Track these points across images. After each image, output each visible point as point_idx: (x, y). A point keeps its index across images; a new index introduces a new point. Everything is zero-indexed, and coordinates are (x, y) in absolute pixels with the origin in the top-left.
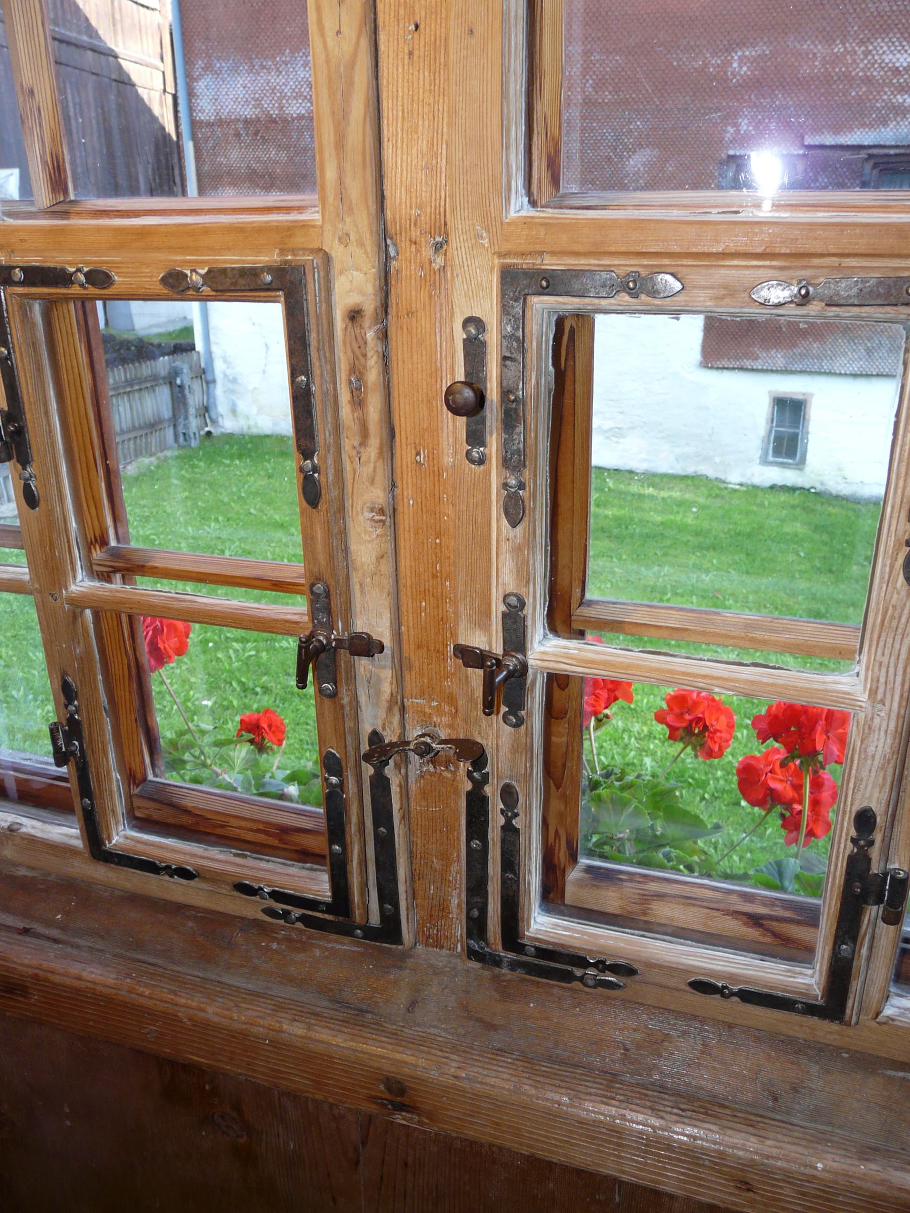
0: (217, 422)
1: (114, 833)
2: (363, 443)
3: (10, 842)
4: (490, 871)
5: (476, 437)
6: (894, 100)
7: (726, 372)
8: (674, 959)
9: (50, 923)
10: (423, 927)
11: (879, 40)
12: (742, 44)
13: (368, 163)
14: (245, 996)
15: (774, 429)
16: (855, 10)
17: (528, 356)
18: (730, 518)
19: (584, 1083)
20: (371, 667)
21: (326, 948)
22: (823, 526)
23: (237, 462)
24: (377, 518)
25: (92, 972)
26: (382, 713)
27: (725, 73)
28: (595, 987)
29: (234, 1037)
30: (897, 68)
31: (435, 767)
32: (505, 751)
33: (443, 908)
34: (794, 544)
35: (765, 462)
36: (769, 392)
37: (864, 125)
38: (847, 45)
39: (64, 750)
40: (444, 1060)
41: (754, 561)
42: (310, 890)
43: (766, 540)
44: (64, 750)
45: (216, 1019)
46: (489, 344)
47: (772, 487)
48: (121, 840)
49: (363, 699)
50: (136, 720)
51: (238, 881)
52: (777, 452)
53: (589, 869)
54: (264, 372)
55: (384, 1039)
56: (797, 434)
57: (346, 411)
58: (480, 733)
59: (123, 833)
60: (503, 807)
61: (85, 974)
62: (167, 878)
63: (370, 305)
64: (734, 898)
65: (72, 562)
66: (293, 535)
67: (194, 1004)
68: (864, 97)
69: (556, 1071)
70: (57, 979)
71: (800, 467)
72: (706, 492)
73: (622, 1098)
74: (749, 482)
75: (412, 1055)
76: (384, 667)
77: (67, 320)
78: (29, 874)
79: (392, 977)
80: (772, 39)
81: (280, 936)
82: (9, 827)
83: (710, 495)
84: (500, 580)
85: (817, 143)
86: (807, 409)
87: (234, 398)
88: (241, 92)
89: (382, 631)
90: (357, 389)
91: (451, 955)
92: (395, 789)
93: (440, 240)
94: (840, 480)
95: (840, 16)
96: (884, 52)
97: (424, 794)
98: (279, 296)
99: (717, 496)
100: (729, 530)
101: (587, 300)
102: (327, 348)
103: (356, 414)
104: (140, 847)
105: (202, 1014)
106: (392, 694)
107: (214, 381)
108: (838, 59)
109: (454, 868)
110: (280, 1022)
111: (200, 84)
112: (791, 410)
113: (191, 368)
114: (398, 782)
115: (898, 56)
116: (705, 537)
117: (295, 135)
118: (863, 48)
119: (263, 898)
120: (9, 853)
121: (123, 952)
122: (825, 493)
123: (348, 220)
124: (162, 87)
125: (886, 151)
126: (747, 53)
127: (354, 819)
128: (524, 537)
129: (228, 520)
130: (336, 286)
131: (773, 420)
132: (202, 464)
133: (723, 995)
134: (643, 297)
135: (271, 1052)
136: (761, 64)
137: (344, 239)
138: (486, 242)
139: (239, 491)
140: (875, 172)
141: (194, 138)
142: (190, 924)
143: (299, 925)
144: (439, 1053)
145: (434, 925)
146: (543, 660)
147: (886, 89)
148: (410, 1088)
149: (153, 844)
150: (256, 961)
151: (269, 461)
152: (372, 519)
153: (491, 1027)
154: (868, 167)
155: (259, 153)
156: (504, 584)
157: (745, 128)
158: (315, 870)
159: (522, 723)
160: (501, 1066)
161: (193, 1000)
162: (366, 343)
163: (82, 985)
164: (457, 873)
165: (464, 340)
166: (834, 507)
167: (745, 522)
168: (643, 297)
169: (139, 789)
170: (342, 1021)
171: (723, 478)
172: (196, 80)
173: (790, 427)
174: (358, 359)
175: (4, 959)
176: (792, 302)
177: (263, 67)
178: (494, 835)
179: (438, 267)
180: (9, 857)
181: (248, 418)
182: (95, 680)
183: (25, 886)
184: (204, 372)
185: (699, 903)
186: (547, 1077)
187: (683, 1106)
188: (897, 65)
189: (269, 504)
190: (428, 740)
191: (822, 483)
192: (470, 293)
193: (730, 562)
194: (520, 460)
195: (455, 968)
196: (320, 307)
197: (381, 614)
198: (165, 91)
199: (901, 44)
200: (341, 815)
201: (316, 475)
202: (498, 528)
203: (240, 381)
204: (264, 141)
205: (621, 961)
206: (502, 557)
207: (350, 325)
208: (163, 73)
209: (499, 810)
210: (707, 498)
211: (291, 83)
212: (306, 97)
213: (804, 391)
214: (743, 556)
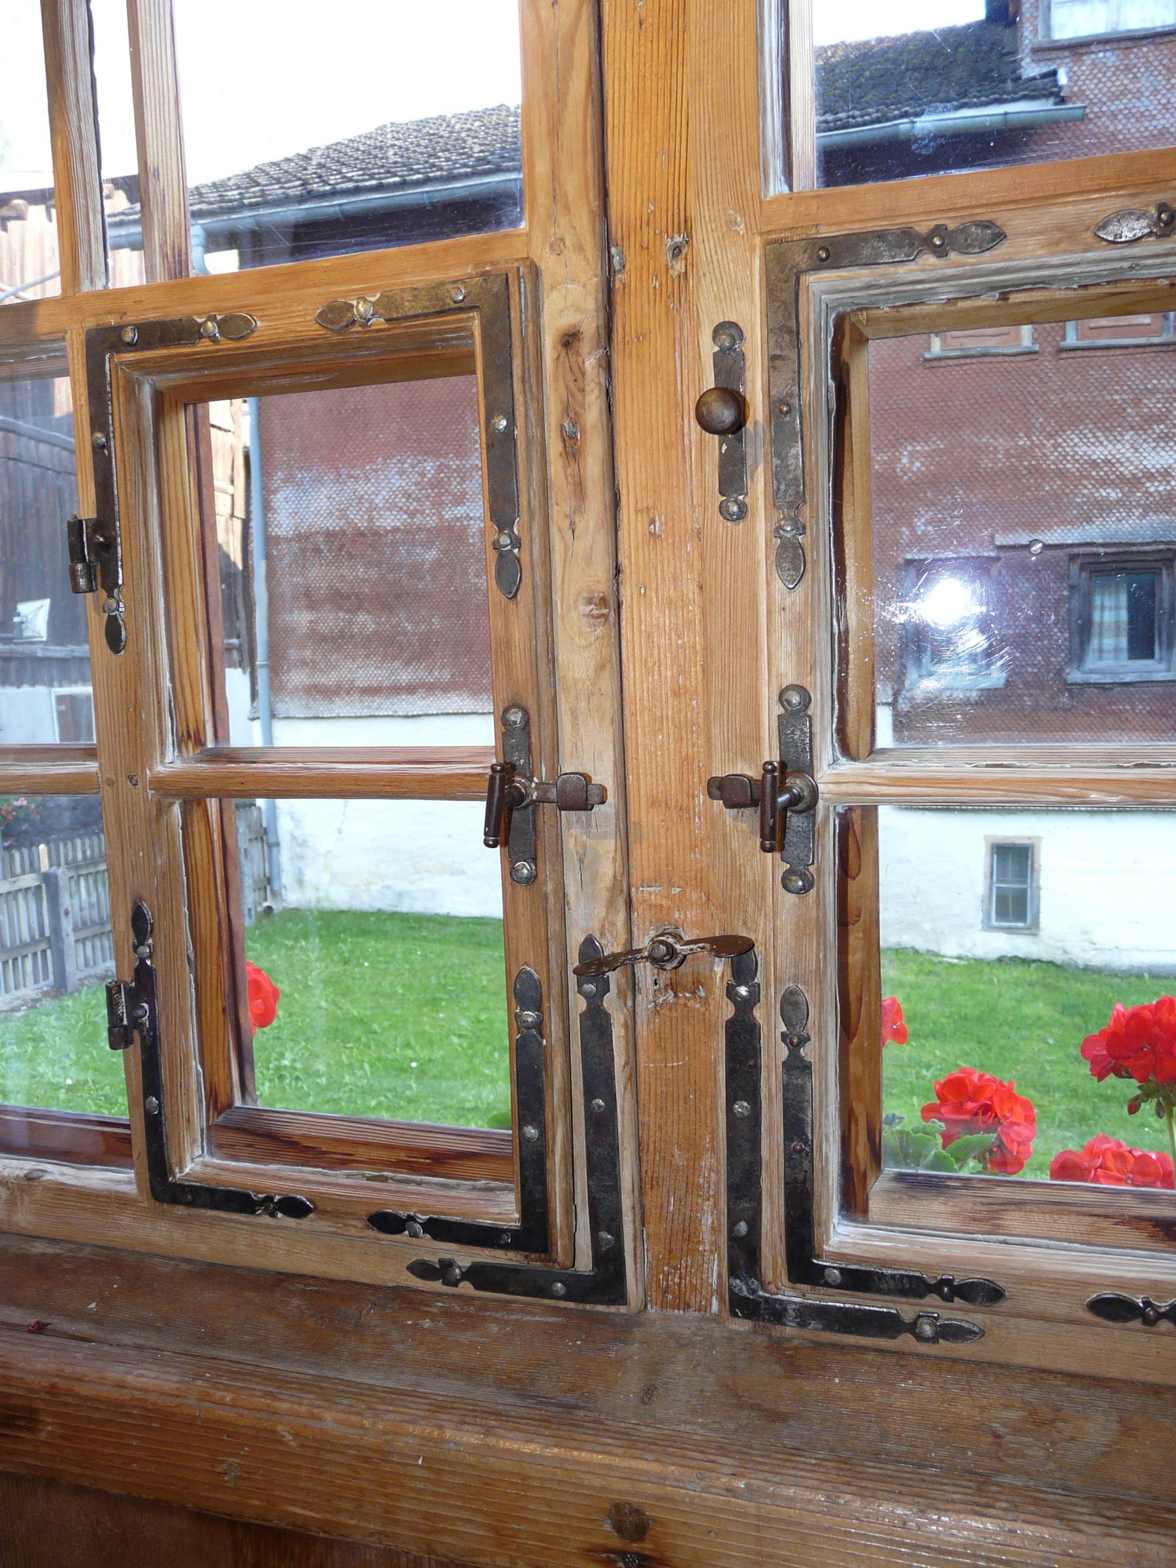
0: (280, 894)
1: (188, 1158)
2: (579, 509)
3: (26, 1198)
4: (765, 1153)
5: (732, 477)
6: (1097, 495)
7: (928, 815)
8: (1060, 1268)
9: (79, 1315)
10: (658, 1274)
11: (1069, 432)
12: (913, 439)
13: (589, 148)
14: (383, 1395)
15: (995, 885)
16: (1036, 402)
17: (804, 352)
18: (950, 999)
19: (939, 1487)
20: (584, 837)
21: (507, 1322)
22: (1074, 1006)
23: (303, 943)
24: (595, 612)
25: (142, 1376)
26: (600, 911)
27: (894, 471)
28: (934, 1340)
29: (366, 1460)
30: (1094, 461)
31: (676, 996)
32: (786, 936)
33: (689, 1235)
34: (1039, 1028)
35: (988, 927)
36: (986, 837)
37: (1062, 523)
38: (1034, 438)
39: (125, 1022)
40: (708, 1465)
41: (989, 1050)
42: (487, 1213)
43: (1001, 1026)
44: (125, 1022)
45: (338, 1430)
46: (748, 356)
47: (1000, 960)
48: (198, 1168)
49: (572, 889)
50: (224, 1010)
51: (374, 1210)
52: (1002, 914)
53: (900, 1178)
54: (340, 831)
55: (608, 1441)
56: (1025, 890)
57: (556, 466)
58: (745, 923)
59: (201, 1159)
60: (784, 1029)
61: (130, 1379)
62: (266, 1219)
63: (590, 325)
64: (1127, 1201)
65: (161, 733)
66: (376, 1033)
67: (303, 1409)
68: (1059, 492)
69: (890, 1473)
70: (83, 1390)
71: (1034, 931)
72: (915, 968)
73: (1003, 1505)
74: (970, 955)
75: (657, 1461)
76: (605, 836)
77: (176, 439)
78: (51, 1250)
79: (612, 1355)
80: (946, 433)
81: (434, 1310)
82: (26, 1176)
83: (921, 971)
84: (774, 670)
85: (1011, 543)
86: (1036, 856)
87: (301, 864)
88: (324, 504)
89: (604, 775)
90: (571, 438)
91: (702, 1319)
92: (618, 1032)
93: (680, 239)
94: (1087, 946)
95: (1020, 407)
96: (1075, 445)
97: (660, 1041)
98: (473, 318)
99: (930, 972)
100: (951, 1013)
101: (880, 270)
102: (533, 380)
103: (569, 471)
104: (226, 1176)
105: (316, 1424)
106: (615, 877)
107: (278, 844)
108: (1025, 453)
109: (707, 1161)
110: (440, 1427)
111: (278, 496)
112: (1014, 859)
113: (249, 827)
114: (622, 1020)
115: (1093, 448)
116: (921, 1024)
117: (388, 550)
118: (1052, 442)
119: (414, 1235)
120: (23, 1218)
121: (189, 1347)
122: (1069, 964)
123: (562, 221)
124: (229, 511)
125: (1094, 549)
126: (919, 448)
127: (558, 1082)
128: (806, 604)
129: (290, 1015)
130: (546, 306)
131: (992, 873)
132: (258, 946)
133: (1149, 1322)
134: (953, 256)
135: (427, 1480)
136: (937, 459)
137: (557, 246)
138: (741, 229)
139: (306, 979)
140: (1084, 575)
141: (268, 557)
142: (295, 1302)
143: (466, 1288)
144: (701, 1456)
145: (675, 1268)
146: (838, 783)
147: (1086, 482)
148: (655, 1520)
149: (246, 1172)
150: (399, 1347)
151: (345, 942)
152: (590, 615)
153: (778, 1417)
154: (1074, 568)
155: (344, 571)
156: (779, 675)
157: (923, 528)
158: (493, 1189)
159: (812, 885)
160: (802, 1470)
161: (301, 1404)
162: (583, 374)
163: (126, 1395)
164: (710, 1170)
165: (715, 355)
166: (1082, 983)
167: (970, 1003)
168: (953, 256)
169: (221, 1118)
170: (539, 1420)
171: (936, 950)
172: (274, 492)
173: (1014, 882)
174: (573, 395)
175: (5, 1366)
176: (1150, 234)
177: (350, 476)
178: (771, 1083)
179: (676, 273)
180: (23, 1224)
181: (317, 889)
182: (179, 912)
183: (44, 1268)
184: (266, 832)
185: (1075, 1209)
186: (877, 1481)
187: (1108, 1513)
188: (1094, 457)
189: (344, 995)
190: (671, 940)
191: (1065, 952)
192: (722, 295)
193: (958, 1052)
194: (798, 493)
195: (711, 1336)
196: (526, 327)
197: (600, 754)
198: (232, 515)
199: (1094, 436)
200: (537, 1074)
201: (516, 551)
202: (769, 593)
203: (310, 844)
204: (351, 556)
205: (976, 1277)
206: (776, 636)
207: (563, 353)
208: (233, 496)
209: (779, 1035)
210: (917, 975)
211: (384, 493)
212: (401, 509)
213: (1030, 834)
214: (973, 1045)
